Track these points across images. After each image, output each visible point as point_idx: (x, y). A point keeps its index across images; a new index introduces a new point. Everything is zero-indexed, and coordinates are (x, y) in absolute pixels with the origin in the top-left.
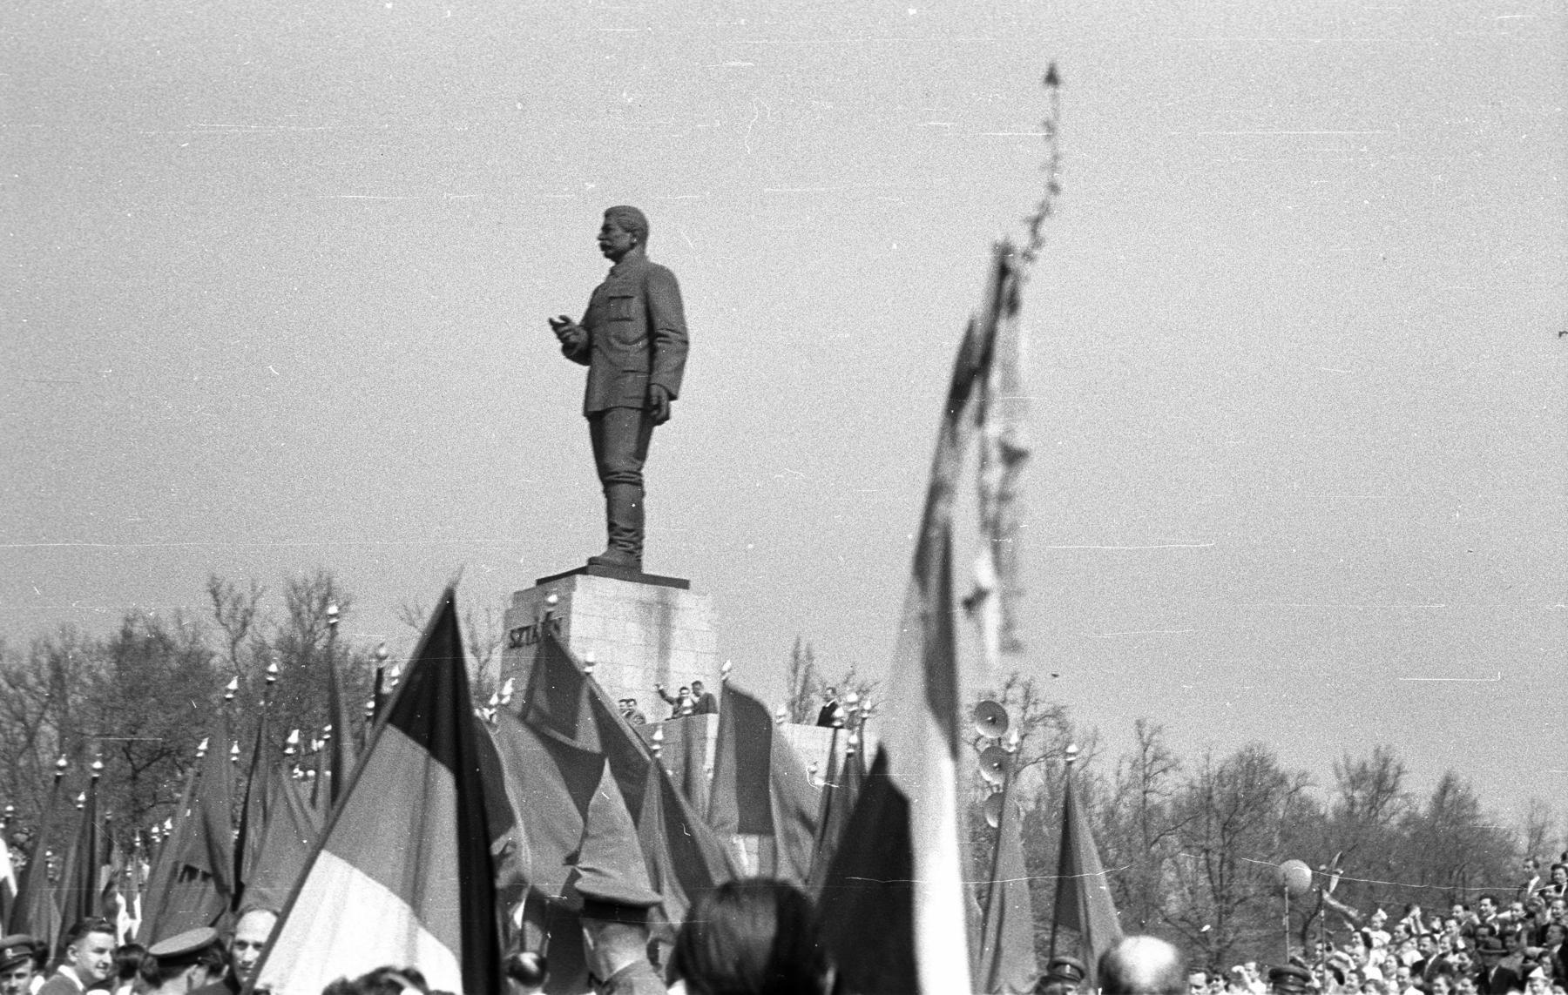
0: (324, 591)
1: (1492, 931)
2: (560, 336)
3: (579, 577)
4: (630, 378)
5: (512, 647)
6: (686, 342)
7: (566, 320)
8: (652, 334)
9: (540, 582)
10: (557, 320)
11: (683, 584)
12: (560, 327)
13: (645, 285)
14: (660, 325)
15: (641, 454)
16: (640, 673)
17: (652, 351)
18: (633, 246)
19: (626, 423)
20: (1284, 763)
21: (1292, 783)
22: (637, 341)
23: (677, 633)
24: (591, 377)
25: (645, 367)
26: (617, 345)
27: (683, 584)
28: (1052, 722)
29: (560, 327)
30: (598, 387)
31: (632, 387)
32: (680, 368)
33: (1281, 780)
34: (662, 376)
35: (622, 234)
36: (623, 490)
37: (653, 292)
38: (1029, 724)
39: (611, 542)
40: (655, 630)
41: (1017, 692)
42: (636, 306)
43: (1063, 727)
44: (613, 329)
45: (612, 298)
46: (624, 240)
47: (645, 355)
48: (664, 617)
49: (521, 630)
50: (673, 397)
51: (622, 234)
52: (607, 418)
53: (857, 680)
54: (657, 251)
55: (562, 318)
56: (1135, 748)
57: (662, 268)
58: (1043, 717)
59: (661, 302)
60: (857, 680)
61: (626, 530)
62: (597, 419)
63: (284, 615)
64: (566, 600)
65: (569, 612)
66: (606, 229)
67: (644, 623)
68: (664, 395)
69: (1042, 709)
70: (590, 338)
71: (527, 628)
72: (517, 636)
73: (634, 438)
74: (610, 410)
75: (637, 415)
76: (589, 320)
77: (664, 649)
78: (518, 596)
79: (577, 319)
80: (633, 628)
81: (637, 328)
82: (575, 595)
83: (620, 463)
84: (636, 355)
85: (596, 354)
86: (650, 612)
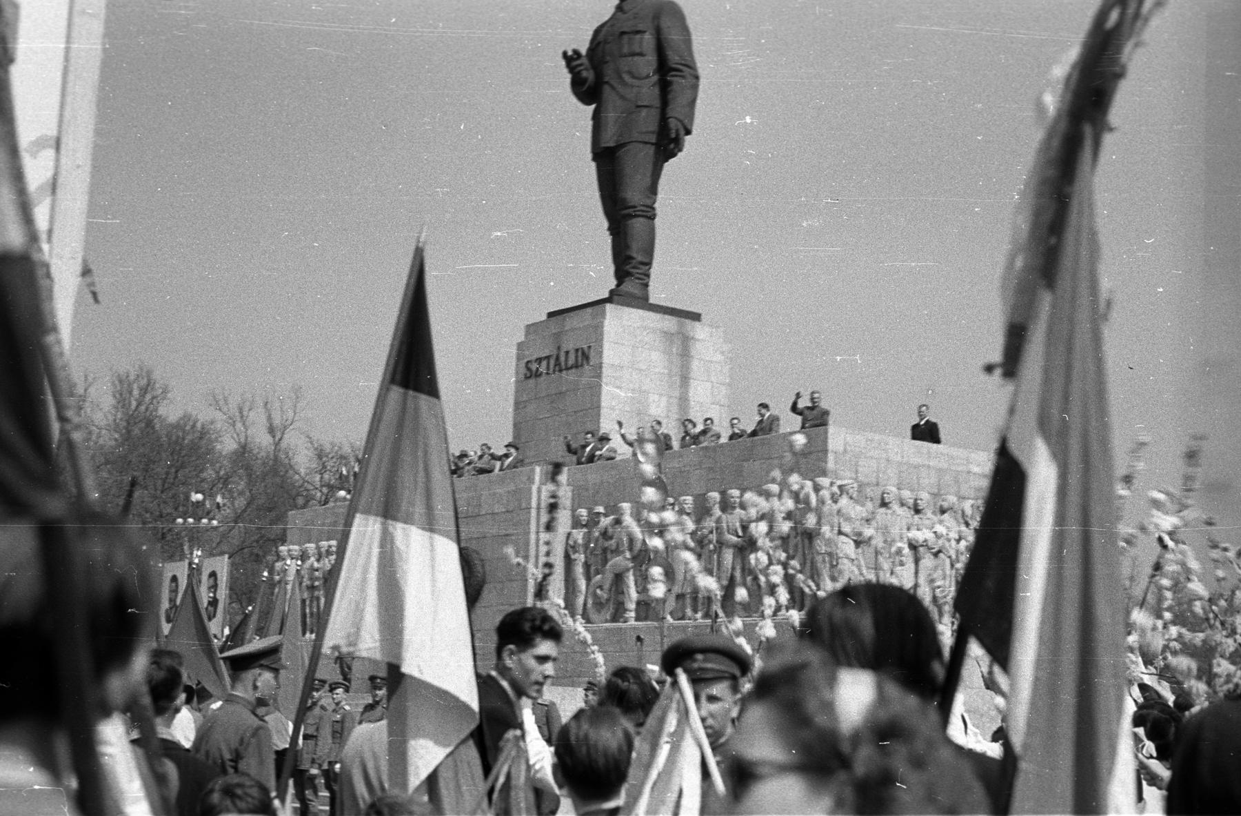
0: (144, 382)
2: (571, 69)
3: (608, 306)
4: (644, 112)
5: (527, 378)
6: (697, 78)
7: (576, 52)
9: (551, 315)
11: (696, 317)
13: (657, 17)
15: (653, 190)
16: (664, 399)
17: (665, 87)
19: (637, 158)
22: (648, 77)
23: (695, 365)
24: (596, 117)
25: (657, 103)
26: (627, 78)
27: (696, 317)
29: (571, 60)
32: (692, 103)
34: (676, 110)
37: (665, 31)
40: (677, 361)
42: (648, 39)
44: (624, 64)
45: (623, 33)
47: (656, 91)
48: (682, 349)
49: (539, 360)
50: (688, 132)
52: (621, 152)
57: (597, 32)
59: (673, 36)
62: (607, 159)
63: (108, 402)
64: (598, 329)
65: (599, 340)
67: (667, 352)
71: (548, 358)
72: (534, 366)
73: (649, 174)
75: (651, 150)
77: (685, 380)
78: (531, 329)
79: (583, 51)
80: (656, 356)
81: (647, 64)
82: (606, 322)
84: (648, 92)
85: (607, 90)
86: (672, 342)
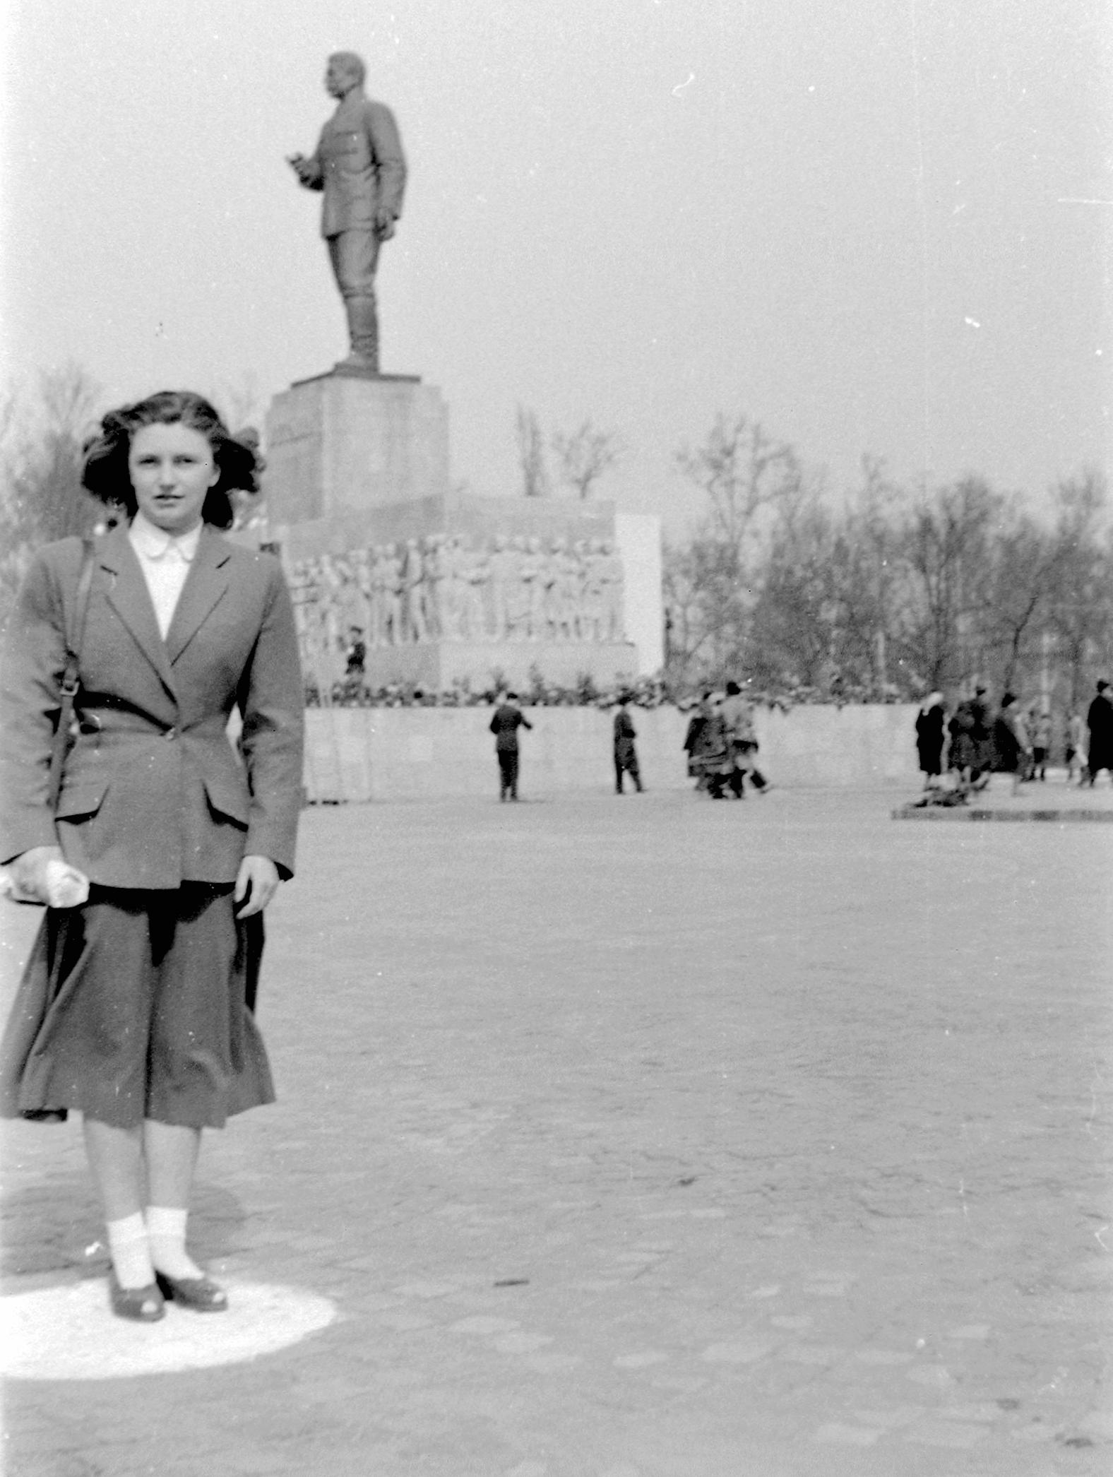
1: (1078, 587)
7: (300, 159)
8: (375, 161)
10: (728, 792)
12: (296, 162)
14: (382, 156)
15: (372, 268)
18: (353, 86)
19: (355, 246)
20: (998, 485)
21: (1008, 501)
28: (782, 461)
29: (296, 162)
30: (332, 215)
31: (361, 212)
32: (400, 194)
33: (999, 501)
34: (387, 199)
35: (345, 77)
36: (357, 301)
38: (760, 465)
39: (353, 347)
41: (747, 436)
42: (358, 140)
43: (792, 463)
46: (346, 82)
50: (396, 218)
51: (345, 77)
52: (341, 239)
53: (593, 432)
54: (376, 90)
55: (718, 794)
56: (860, 482)
58: (772, 457)
60: (593, 432)
61: (365, 331)
63: (40, 409)
66: (331, 73)
68: (388, 218)
69: (773, 448)
70: (322, 168)
74: (343, 232)
76: (321, 157)
83: (355, 281)
